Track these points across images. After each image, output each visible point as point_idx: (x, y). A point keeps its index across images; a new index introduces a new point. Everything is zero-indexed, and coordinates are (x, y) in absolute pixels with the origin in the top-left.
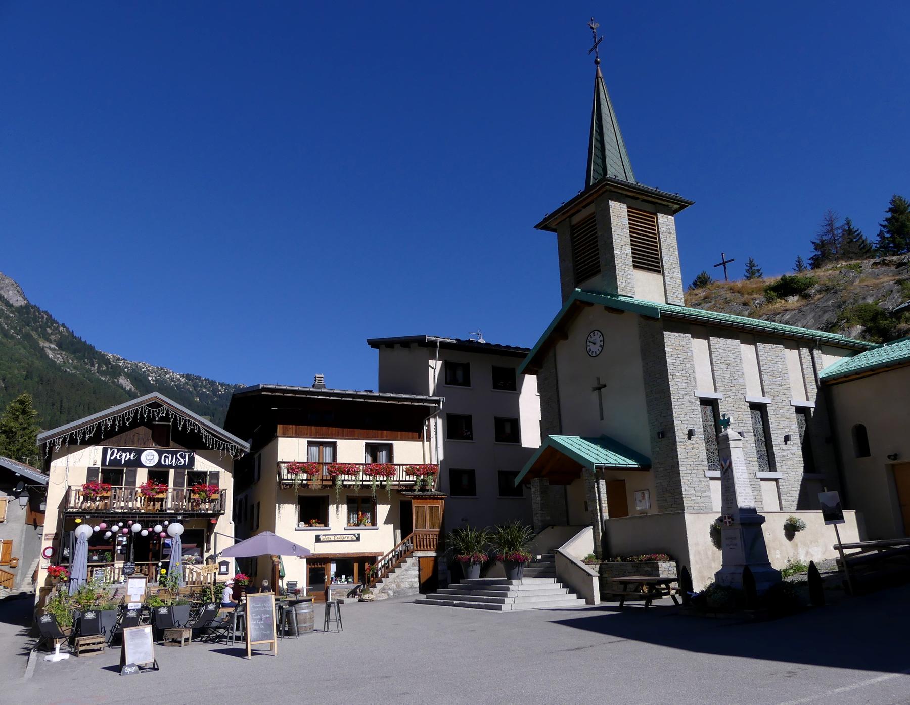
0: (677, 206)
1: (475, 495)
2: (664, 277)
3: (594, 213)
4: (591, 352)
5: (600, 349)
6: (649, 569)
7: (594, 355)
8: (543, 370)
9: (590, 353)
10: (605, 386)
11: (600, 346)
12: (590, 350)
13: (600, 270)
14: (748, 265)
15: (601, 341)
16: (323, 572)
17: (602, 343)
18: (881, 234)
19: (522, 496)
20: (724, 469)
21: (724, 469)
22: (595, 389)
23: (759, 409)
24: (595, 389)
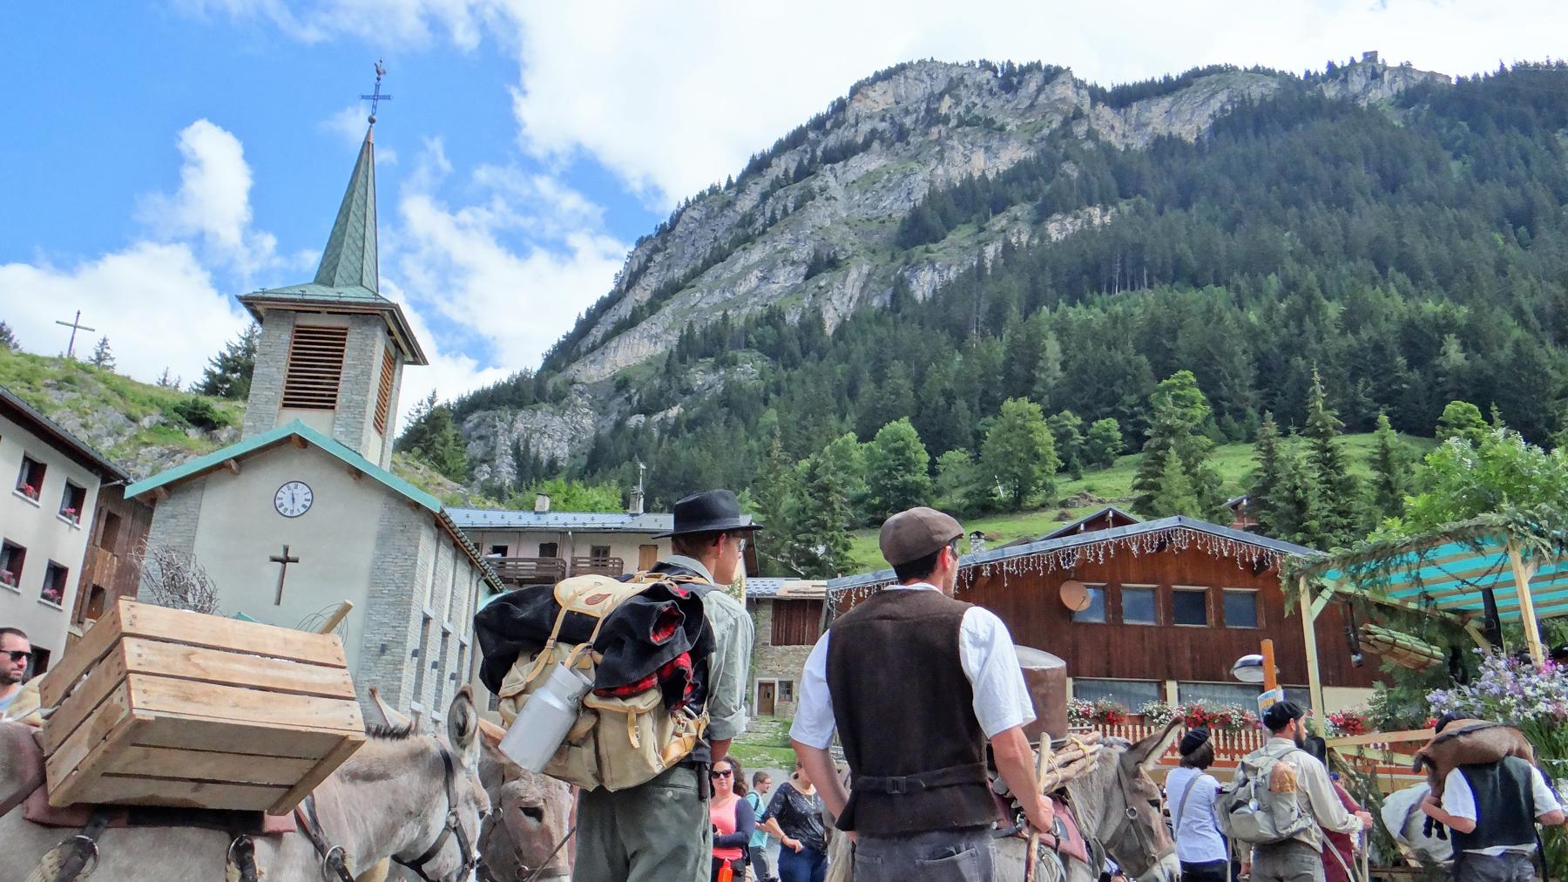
0: (411, 359)
3: (346, 329)
9: (281, 510)
10: (296, 561)
11: (304, 506)
15: (306, 500)
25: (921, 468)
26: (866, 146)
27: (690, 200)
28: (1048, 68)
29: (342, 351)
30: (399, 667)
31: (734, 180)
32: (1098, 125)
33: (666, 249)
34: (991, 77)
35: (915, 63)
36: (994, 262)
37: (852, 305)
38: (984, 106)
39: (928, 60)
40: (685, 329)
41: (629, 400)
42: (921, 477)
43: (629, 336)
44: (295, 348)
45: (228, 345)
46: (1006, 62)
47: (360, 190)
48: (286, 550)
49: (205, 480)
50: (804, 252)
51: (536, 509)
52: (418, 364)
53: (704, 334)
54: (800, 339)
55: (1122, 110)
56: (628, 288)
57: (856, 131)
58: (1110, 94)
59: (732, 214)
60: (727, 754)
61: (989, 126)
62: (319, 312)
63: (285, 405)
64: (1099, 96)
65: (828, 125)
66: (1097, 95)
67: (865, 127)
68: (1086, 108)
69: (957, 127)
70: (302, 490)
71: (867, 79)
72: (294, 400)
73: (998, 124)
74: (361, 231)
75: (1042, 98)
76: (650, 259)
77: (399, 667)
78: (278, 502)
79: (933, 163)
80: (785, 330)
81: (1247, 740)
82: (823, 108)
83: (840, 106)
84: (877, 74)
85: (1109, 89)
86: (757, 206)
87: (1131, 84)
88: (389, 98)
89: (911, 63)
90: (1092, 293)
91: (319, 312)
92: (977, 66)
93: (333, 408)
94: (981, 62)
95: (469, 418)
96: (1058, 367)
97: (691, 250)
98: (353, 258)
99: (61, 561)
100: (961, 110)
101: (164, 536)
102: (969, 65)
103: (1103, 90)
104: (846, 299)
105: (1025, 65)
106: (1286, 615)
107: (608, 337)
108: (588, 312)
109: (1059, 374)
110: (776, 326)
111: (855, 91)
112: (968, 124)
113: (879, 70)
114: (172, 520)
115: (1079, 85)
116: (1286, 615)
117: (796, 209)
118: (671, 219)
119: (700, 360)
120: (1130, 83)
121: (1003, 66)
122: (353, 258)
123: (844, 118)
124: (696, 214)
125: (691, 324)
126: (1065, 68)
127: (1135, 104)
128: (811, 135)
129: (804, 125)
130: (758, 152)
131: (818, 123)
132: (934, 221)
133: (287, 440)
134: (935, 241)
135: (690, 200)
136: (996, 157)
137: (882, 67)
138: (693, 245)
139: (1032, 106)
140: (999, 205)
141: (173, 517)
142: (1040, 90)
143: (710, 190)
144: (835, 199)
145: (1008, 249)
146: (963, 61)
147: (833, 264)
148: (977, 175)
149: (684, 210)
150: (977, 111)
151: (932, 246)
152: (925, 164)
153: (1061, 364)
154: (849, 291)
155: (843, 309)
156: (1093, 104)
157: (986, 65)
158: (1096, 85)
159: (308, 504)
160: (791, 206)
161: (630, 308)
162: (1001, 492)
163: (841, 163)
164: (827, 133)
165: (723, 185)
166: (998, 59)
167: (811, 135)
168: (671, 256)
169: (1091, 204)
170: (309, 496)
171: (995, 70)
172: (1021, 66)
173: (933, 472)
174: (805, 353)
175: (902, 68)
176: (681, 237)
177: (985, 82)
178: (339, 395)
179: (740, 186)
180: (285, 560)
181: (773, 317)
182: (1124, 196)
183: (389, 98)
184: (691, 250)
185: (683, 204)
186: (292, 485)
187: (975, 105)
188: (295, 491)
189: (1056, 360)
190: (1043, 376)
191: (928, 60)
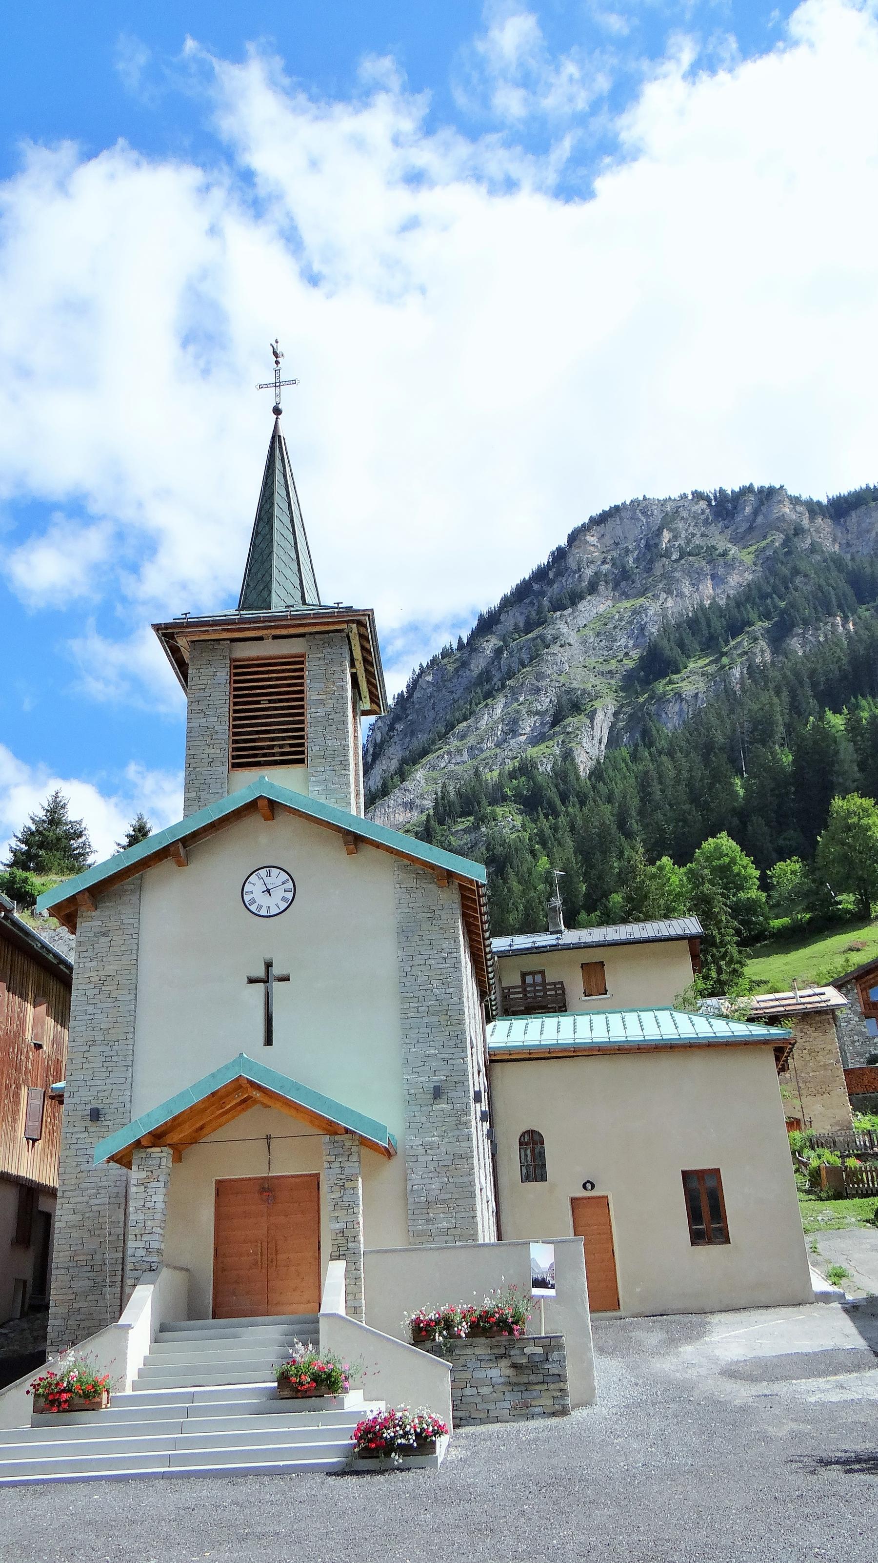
3: (303, 656)
5: (284, 905)
8: (97, 913)
9: (253, 908)
11: (284, 899)
12: (253, 901)
16: (347, 773)
25: (754, 884)
26: (593, 588)
27: (425, 665)
28: (761, 490)
29: (302, 685)
30: (464, 1119)
31: (465, 641)
32: (820, 537)
33: (407, 717)
34: (705, 506)
35: (628, 503)
36: (742, 682)
37: (603, 747)
38: (703, 535)
39: (641, 498)
40: (439, 790)
42: (754, 893)
43: (383, 805)
44: (236, 689)
45: (33, 819)
46: (718, 489)
47: (279, 489)
48: (269, 965)
49: (141, 878)
50: (545, 702)
53: (459, 794)
54: (556, 786)
55: (842, 520)
57: (580, 576)
58: (826, 506)
59: (468, 673)
60: (129, 1253)
61: (711, 555)
62: (261, 639)
63: (235, 766)
64: (816, 508)
65: (551, 575)
66: (814, 508)
67: (589, 572)
68: (805, 522)
69: (681, 558)
70: (277, 878)
71: (583, 525)
73: (720, 551)
74: (291, 538)
75: (760, 519)
77: (464, 1119)
78: (247, 898)
79: (663, 595)
80: (540, 778)
82: (543, 559)
83: (559, 555)
84: (591, 519)
85: (825, 501)
87: (846, 494)
88: (294, 382)
89: (624, 504)
90: (856, 698)
91: (261, 639)
92: (690, 497)
93: (302, 761)
94: (693, 493)
96: (856, 769)
97: (432, 714)
98: (288, 573)
100: (681, 542)
101: (94, 963)
102: (682, 498)
103: (819, 503)
104: (596, 741)
105: (737, 489)
109: (858, 775)
110: (531, 777)
111: (573, 538)
112: (690, 554)
113: (594, 515)
114: (103, 940)
115: (795, 501)
118: (408, 686)
119: (459, 820)
120: (844, 492)
121: (715, 494)
122: (288, 573)
123: (566, 566)
124: (430, 678)
125: (444, 786)
126: (778, 487)
127: (853, 514)
128: (536, 587)
129: (527, 578)
130: (484, 610)
131: (540, 575)
132: (670, 650)
133: (251, 807)
134: (678, 672)
135: (425, 665)
136: (723, 583)
137: (596, 511)
138: (433, 709)
139: (751, 529)
140: (736, 629)
141: (105, 934)
142: (756, 512)
143: (442, 654)
144: (570, 645)
145: (752, 670)
146: (675, 495)
147: (576, 708)
148: (707, 603)
149: (419, 676)
150: (697, 541)
151: (675, 677)
152: (656, 597)
153: (858, 765)
154: (597, 734)
155: (594, 752)
156: (812, 519)
157: (698, 496)
158: (811, 500)
159: (290, 895)
161: (378, 778)
162: (847, 901)
163: (570, 610)
164: (551, 583)
165: (455, 646)
166: (709, 487)
167: (536, 587)
168: (412, 722)
169: (831, 614)
170: (290, 885)
171: (708, 499)
172: (733, 492)
173: (765, 885)
174: (564, 799)
175: (616, 511)
176: (420, 703)
177: (699, 511)
178: (308, 745)
179: (469, 647)
181: (525, 769)
182: (862, 601)
183: (294, 382)
184: (432, 714)
185: (417, 671)
186: (263, 872)
187: (694, 535)
188: (268, 880)
189: (851, 761)
190: (841, 780)
191: (641, 498)
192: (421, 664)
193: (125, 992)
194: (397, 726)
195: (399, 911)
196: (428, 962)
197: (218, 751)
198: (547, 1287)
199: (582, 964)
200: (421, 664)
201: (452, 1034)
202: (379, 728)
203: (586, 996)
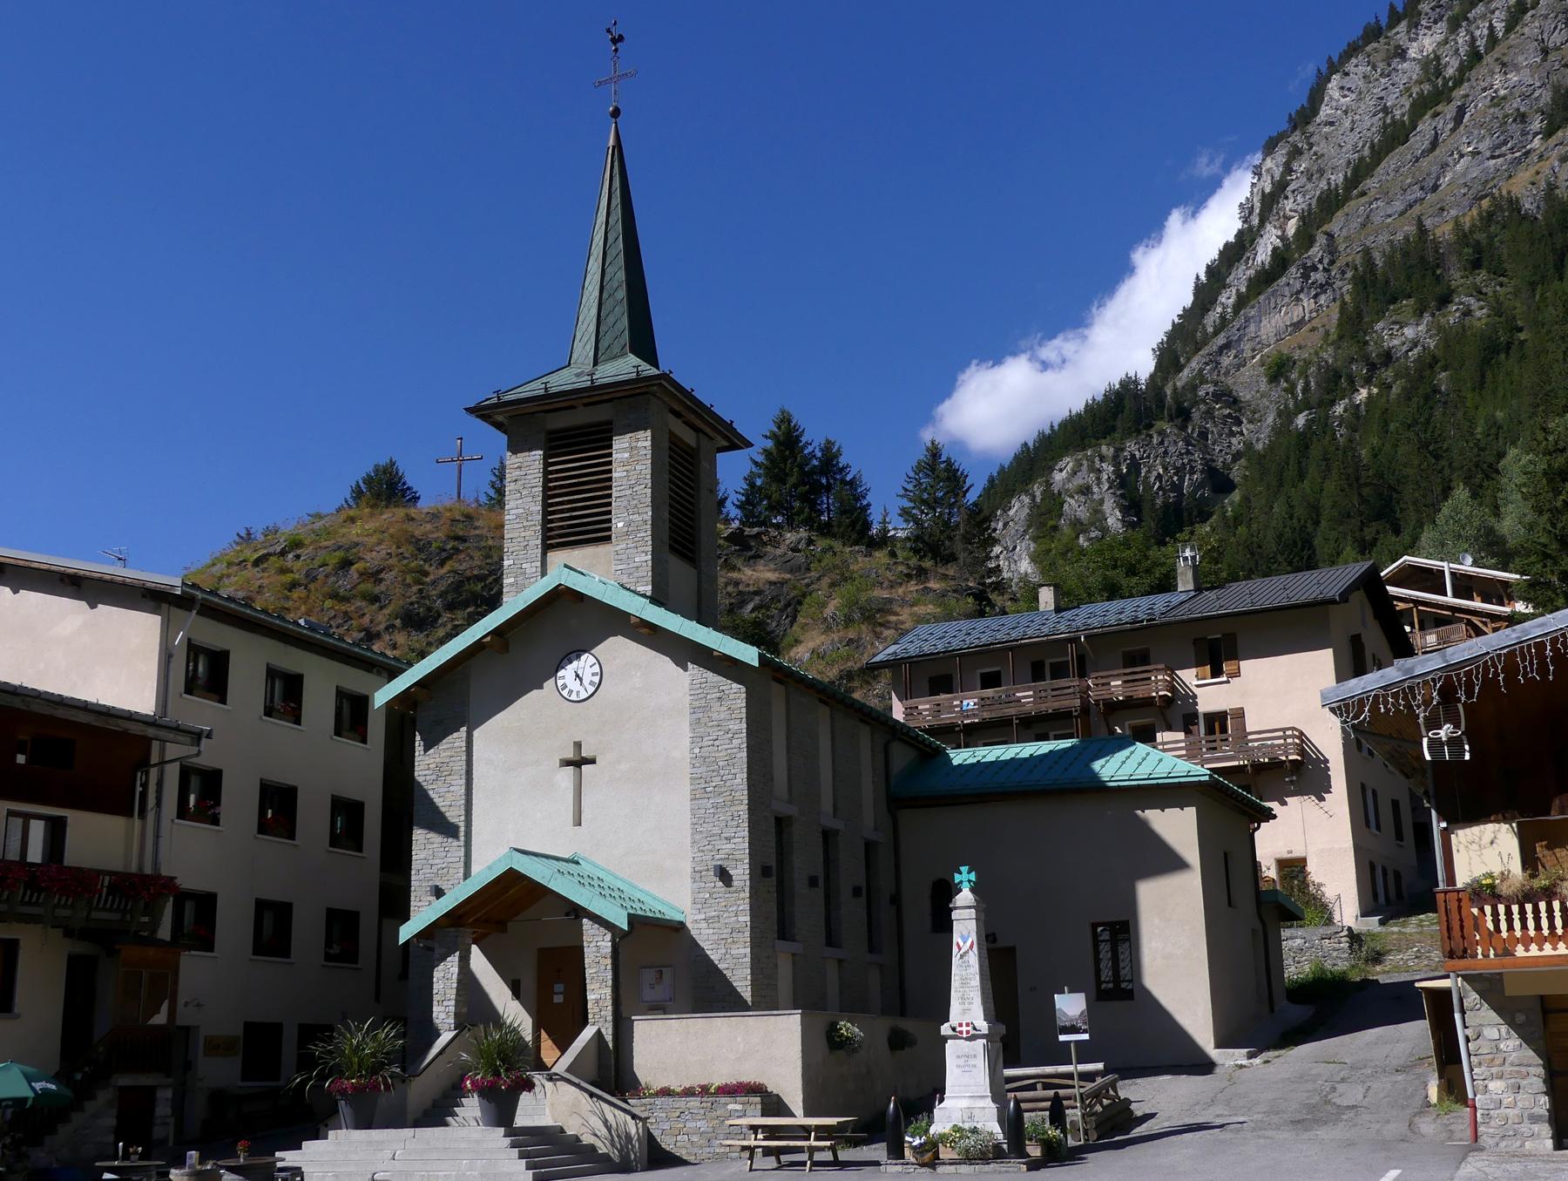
0: (725, 443)
1: (288, 955)
2: (699, 573)
4: (567, 690)
6: (739, 1107)
7: (574, 697)
9: (565, 693)
10: (592, 761)
11: (592, 683)
12: (565, 686)
13: (610, 536)
14: (496, 472)
15: (593, 675)
17: (596, 679)
18: (750, 480)
19: (357, 963)
20: (961, 952)
21: (961, 952)
22: (567, 763)
23: (828, 836)
24: (567, 763)
33: (1310, 149)
41: (1291, 390)
48: (578, 745)
51: (10, 818)
52: (737, 448)
56: (1263, 220)
72: (556, 536)
76: (1288, 169)
81: (1537, 919)
86: (1446, 42)
93: (608, 538)
95: (1061, 464)
99: (351, 792)
106: (1299, 758)
107: (1242, 302)
108: (1210, 270)
116: (1299, 758)
117: (1509, 29)
125: (1367, 252)
160: (1499, 26)
180: (578, 762)
192: (1330, 57)
193: (458, 777)
194: (1295, 166)
195: (692, 692)
196: (717, 743)
197: (533, 533)
198: (1079, 1033)
199: (1195, 640)
200: (1330, 57)
201: (735, 814)
202: (1268, 171)
203: (1198, 680)
